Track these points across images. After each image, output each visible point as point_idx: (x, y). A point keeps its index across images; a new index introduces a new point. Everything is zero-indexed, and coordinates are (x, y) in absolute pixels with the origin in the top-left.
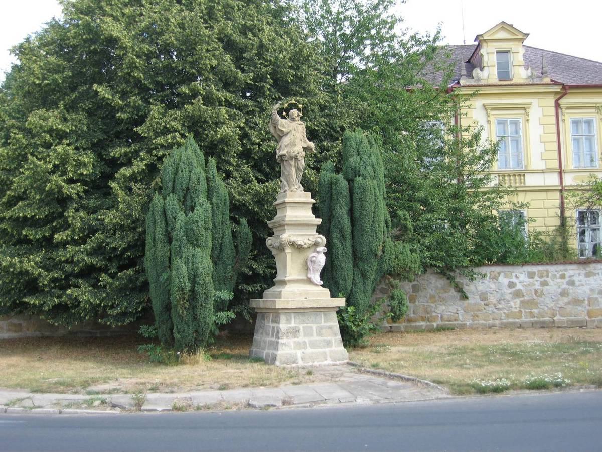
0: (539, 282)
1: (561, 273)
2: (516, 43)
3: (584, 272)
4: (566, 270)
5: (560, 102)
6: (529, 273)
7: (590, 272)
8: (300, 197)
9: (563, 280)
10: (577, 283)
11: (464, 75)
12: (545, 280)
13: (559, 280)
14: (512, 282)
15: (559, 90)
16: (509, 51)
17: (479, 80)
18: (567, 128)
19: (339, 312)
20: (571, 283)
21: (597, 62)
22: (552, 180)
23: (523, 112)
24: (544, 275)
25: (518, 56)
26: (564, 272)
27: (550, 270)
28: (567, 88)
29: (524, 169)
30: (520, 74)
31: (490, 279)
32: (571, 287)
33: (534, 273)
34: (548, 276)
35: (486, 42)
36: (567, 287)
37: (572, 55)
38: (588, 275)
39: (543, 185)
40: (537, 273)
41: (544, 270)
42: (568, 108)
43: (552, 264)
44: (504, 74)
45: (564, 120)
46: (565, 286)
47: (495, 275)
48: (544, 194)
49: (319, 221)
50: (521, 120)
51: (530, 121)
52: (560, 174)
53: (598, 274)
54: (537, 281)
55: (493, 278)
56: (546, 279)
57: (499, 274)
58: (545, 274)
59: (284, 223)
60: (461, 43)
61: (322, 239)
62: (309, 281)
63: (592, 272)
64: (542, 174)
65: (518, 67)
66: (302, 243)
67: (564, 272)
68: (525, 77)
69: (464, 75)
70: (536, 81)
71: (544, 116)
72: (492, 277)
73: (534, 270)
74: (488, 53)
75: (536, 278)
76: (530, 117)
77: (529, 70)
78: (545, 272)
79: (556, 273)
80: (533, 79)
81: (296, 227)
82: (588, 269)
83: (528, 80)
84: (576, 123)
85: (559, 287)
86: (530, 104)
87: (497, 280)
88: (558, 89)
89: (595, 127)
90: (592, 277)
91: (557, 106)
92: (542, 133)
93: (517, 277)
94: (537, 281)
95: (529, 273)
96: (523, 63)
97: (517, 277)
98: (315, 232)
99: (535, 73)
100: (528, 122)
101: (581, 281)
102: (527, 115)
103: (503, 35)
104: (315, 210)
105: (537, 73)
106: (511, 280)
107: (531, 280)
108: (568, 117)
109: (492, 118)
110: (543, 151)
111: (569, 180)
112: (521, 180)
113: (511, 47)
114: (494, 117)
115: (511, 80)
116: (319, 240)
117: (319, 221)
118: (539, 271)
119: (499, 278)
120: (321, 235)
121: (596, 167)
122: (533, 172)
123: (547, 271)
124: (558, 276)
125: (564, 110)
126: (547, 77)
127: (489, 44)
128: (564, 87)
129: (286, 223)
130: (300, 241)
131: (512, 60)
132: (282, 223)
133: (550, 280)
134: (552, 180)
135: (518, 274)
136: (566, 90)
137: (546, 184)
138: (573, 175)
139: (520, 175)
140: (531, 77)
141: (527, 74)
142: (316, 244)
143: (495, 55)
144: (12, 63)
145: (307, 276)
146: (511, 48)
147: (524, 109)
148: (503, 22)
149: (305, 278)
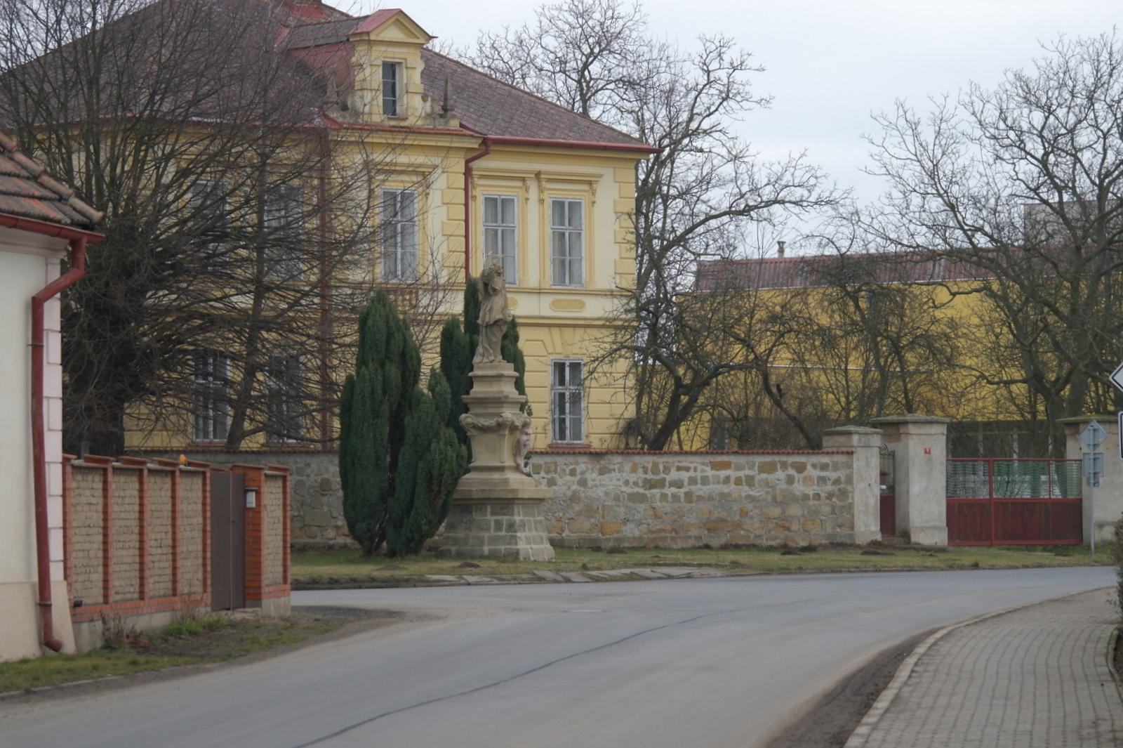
2: (412, 50)
3: (598, 467)
4: (577, 463)
5: (474, 165)
9: (573, 478)
10: (590, 483)
13: (569, 478)
15: (477, 146)
16: (400, 63)
17: (357, 114)
18: (478, 209)
20: (583, 483)
25: (412, 77)
30: (415, 107)
32: (582, 489)
34: (556, 471)
36: (578, 488)
38: (603, 471)
39: (536, 313)
42: (482, 177)
43: (743, 453)
46: (575, 487)
58: (553, 468)
64: (537, 296)
70: (440, 125)
71: (448, 188)
75: (543, 474)
76: (598, 198)
77: (429, 103)
82: (602, 462)
83: (428, 121)
84: (491, 202)
85: (569, 488)
86: (600, 176)
90: (606, 475)
91: (468, 173)
96: (420, 88)
103: (393, 34)
108: (482, 191)
118: (546, 463)
121: (515, 283)
124: (568, 471)
126: (454, 117)
128: (486, 142)
136: (487, 146)
144: (480, 31)
146: (405, 59)
147: (590, 183)
149: (512, 464)
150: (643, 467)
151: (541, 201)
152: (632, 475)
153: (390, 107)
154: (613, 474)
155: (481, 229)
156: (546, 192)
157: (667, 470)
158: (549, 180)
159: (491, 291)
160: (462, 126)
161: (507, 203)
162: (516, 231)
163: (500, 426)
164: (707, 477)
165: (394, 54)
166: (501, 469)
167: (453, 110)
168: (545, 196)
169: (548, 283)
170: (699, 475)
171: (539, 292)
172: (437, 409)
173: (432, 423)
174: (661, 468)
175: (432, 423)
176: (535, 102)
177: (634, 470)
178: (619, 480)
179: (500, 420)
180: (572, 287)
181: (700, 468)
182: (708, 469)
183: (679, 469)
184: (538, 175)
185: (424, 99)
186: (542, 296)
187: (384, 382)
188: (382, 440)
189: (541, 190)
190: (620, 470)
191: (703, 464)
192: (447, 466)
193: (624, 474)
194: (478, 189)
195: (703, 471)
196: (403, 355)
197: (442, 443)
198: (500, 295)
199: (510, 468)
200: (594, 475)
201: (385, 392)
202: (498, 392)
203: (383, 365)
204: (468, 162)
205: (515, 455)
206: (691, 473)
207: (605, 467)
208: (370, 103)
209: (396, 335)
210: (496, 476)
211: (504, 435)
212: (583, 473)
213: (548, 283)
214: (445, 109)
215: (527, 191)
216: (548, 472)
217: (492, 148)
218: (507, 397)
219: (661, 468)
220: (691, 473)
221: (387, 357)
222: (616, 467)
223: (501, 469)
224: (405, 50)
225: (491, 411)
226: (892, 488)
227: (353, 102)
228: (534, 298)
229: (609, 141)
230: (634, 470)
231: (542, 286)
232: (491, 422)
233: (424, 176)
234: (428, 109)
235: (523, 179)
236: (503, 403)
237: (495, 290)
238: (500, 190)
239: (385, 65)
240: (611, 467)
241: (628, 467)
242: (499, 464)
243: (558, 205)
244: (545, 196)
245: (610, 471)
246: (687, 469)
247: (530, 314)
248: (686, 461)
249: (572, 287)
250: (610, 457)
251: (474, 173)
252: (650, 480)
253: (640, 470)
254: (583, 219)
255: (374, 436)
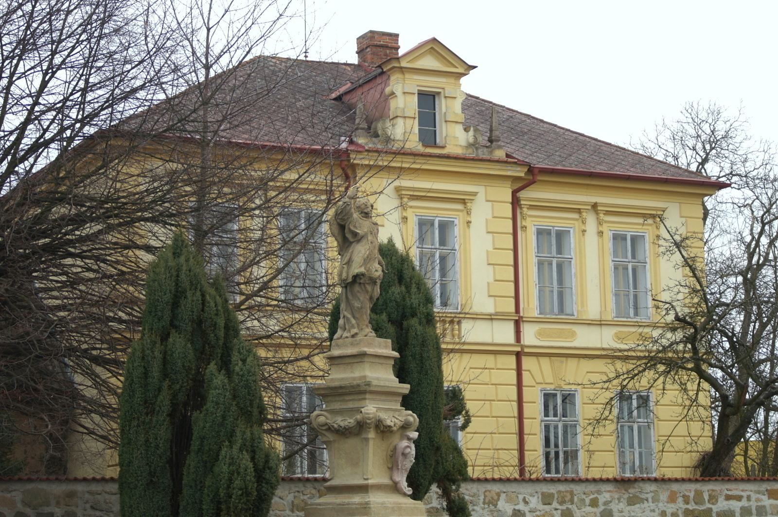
0: (559, 512)
1: (592, 497)
3: (626, 496)
4: (599, 492)
5: (522, 194)
6: (543, 494)
7: (635, 496)
8: (380, 346)
11: (362, 129)
12: (567, 508)
14: (519, 511)
15: (522, 175)
16: (439, 93)
17: (388, 140)
18: (529, 241)
19: (395, 359)
21: (555, 126)
22: (504, 334)
23: (460, 207)
24: (567, 499)
25: (450, 109)
26: (596, 495)
27: (575, 492)
28: (536, 171)
29: (459, 310)
30: (455, 137)
31: (484, 503)
33: (551, 496)
35: (403, 73)
37: (532, 115)
38: (632, 502)
39: (489, 341)
40: (556, 496)
41: (567, 492)
42: (532, 207)
44: (429, 136)
45: (524, 228)
47: (492, 498)
48: (491, 358)
49: (406, 388)
50: (456, 222)
51: (471, 225)
52: (517, 324)
53: (647, 500)
54: (556, 509)
55: (489, 503)
56: (570, 507)
57: (498, 495)
59: (368, 388)
60: (318, 60)
61: (412, 417)
62: (395, 488)
63: (638, 497)
64: (489, 322)
65: (453, 125)
66: (392, 424)
67: (596, 495)
68: (463, 143)
69: (362, 129)
70: (483, 153)
72: (487, 501)
73: (552, 491)
74: (404, 93)
75: (555, 504)
76: (473, 218)
77: (471, 133)
78: (568, 495)
79: (584, 497)
80: (477, 149)
81: (383, 398)
82: (632, 491)
83: (470, 151)
84: (541, 233)
87: (495, 506)
88: (520, 172)
89: (572, 246)
90: (638, 505)
91: (516, 202)
92: (491, 249)
93: (526, 502)
94: (556, 509)
95: (543, 494)
96: (461, 118)
97: (526, 502)
98: (398, 406)
99: (480, 139)
100: (469, 227)
101: (622, 512)
102: (469, 213)
103: (429, 62)
104: (401, 373)
105: (483, 140)
106: (517, 507)
107: (547, 507)
108: (532, 222)
109: (411, 214)
110: (491, 280)
111: (530, 336)
112: (453, 330)
113: (443, 86)
114: (417, 211)
115: (443, 147)
116: (411, 419)
117: (406, 388)
118: (559, 492)
119: (499, 503)
120: (414, 415)
122: (476, 317)
123: (572, 493)
124: (587, 501)
125: (525, 210)
126: (500, 147)
127: (407, 76)
128: (531, 170)
129: (372, 389)
130: (390, 420)
131: (444, 110)
132: (363, 388)
133: (576, 508)
134: (504, 334)
135: (528, 498)
136: (534, 175)
137: (496, 341)
138: (536, 327)
139: (452, 322)
140: (473, 145)
141: (467, 140)
142: (405, 426)
143: (415, 98)
145: (391, 479)
147: (464, 202)
148: (434, 40)
149: (386, 481)
150: (684, 496)
151: (600, 233)
152: (672, 505)
153: (429, 136)
154: (646, 504)
155: (533, 261)
156: (605, 225)
157: (713, 499)
158: (608, 213)
159: (349, 236)
160: (508, 156)
161: (561, 236)
162: (573, 262)
163: (361, 426)
164: (764, 507)
165: (431, 83)
166: (363, 489)
167: (498, 141)
168: (604, 228)
169: (610, 316)
170: (753, 504)
171: (600, 324)
172: (235, 397)
173: (224, 417)
174: (706, 497)
175: (224, 417)
176: (601, 146)
177: (672, 499)
178: (653, 511)
179: (359, 417)
180: (638, 319)
181: (754, 496)
182: (765, 498)
183: (728, 498)
184: (595, 206)
185: (466, 130)
186: (603, 327)
187: (165, 361)
188: (157, 447)
189: (600, 223)
190: (655, 500)
191: (758, 492)
192: (238, 482)
193: (661, 505)
194: (529, 219)
195: (758, 500)
196: (199, 323)
197: (236, 448)
198: (364, 242)
199: (379, 487)
200: (622, 506)
201: (165, 375)
202: (361, 378)
203: (165, 337)
204: (514, 193)
205: (391, 469)
206: (744, 503)
207: (635, 496)
208: (404, 130)
209: (189, 294)
210: (357, 499)
211: (367, 440)
212: (606, 503)
213: (610, 316)
214: (491, 140)
215: (584, 223)
216: (561, 503)
217: (539, 178)
218: (368, 384)
219: (706, 497)
220: (744, 503)
221: (172, 325)
222: (650, 496)
223: (363, 489)
224: (443, 80)
225: (351, 405)
226: (562, 481)
227: (384, 129)
228: (595, 330)
229: (673, 176)
230: (672, 499)
231: (603, 318)
232: (348, 421)
233: (463, 201)
234: (471, 140)
235: (579, 211)
236: (364, 392)
237: (355, 234)
238: (555, 221)
239: (422, 95)
240: (643, 496)
241: (664, 496)
242: (361, 482)
243: (618, 238)
244: (604, 228)
245: (642, 501)
246: (739, 498)
247: (591, 345)
248: (736, 489)
249: (638, 319)
250: (641, 484)
251: (522, 202)
252: (693, 511)
253: (680, 499)
254: (647, 252)
255: (147, 441)
